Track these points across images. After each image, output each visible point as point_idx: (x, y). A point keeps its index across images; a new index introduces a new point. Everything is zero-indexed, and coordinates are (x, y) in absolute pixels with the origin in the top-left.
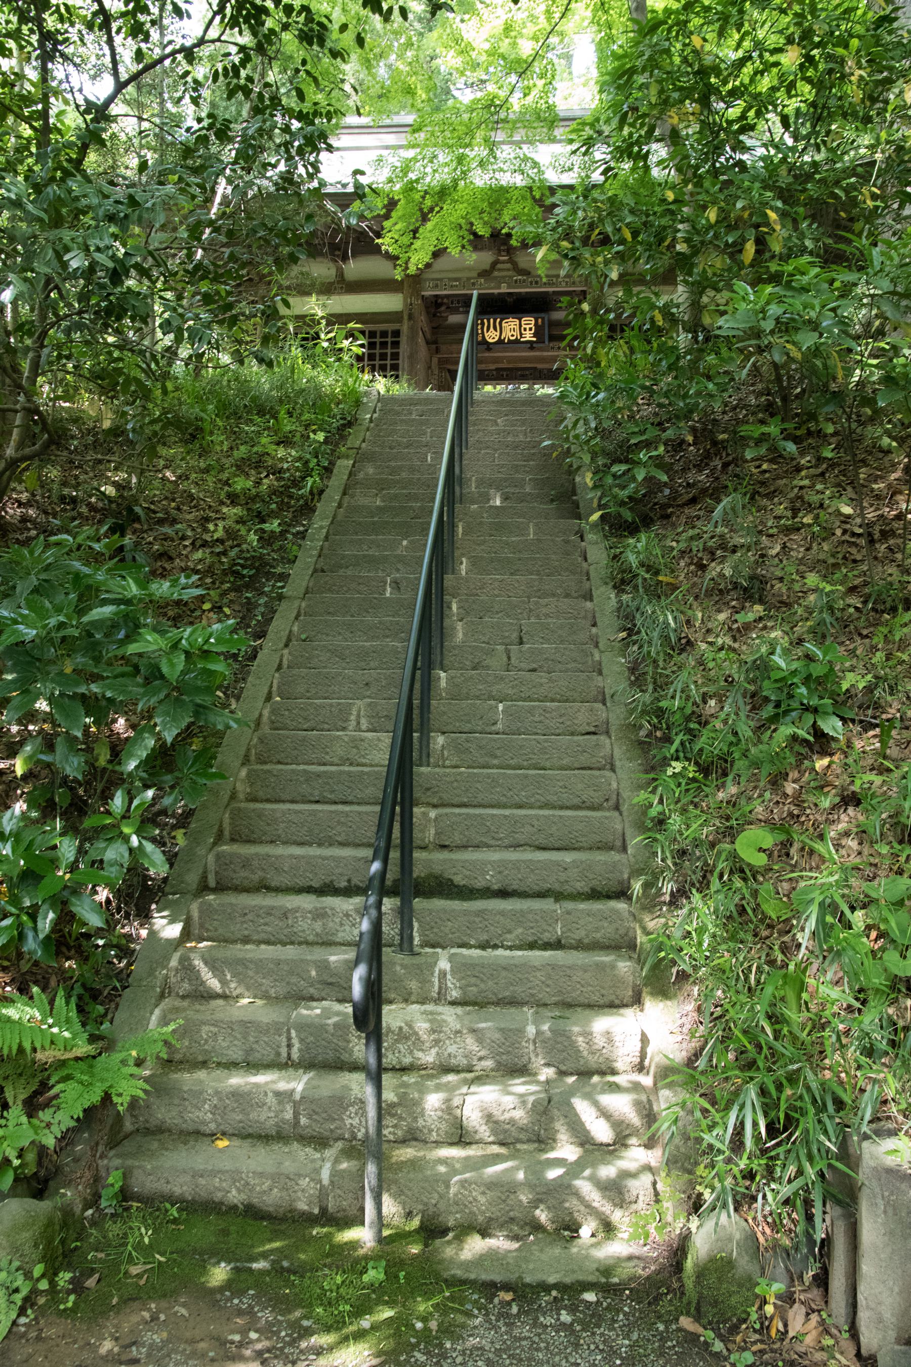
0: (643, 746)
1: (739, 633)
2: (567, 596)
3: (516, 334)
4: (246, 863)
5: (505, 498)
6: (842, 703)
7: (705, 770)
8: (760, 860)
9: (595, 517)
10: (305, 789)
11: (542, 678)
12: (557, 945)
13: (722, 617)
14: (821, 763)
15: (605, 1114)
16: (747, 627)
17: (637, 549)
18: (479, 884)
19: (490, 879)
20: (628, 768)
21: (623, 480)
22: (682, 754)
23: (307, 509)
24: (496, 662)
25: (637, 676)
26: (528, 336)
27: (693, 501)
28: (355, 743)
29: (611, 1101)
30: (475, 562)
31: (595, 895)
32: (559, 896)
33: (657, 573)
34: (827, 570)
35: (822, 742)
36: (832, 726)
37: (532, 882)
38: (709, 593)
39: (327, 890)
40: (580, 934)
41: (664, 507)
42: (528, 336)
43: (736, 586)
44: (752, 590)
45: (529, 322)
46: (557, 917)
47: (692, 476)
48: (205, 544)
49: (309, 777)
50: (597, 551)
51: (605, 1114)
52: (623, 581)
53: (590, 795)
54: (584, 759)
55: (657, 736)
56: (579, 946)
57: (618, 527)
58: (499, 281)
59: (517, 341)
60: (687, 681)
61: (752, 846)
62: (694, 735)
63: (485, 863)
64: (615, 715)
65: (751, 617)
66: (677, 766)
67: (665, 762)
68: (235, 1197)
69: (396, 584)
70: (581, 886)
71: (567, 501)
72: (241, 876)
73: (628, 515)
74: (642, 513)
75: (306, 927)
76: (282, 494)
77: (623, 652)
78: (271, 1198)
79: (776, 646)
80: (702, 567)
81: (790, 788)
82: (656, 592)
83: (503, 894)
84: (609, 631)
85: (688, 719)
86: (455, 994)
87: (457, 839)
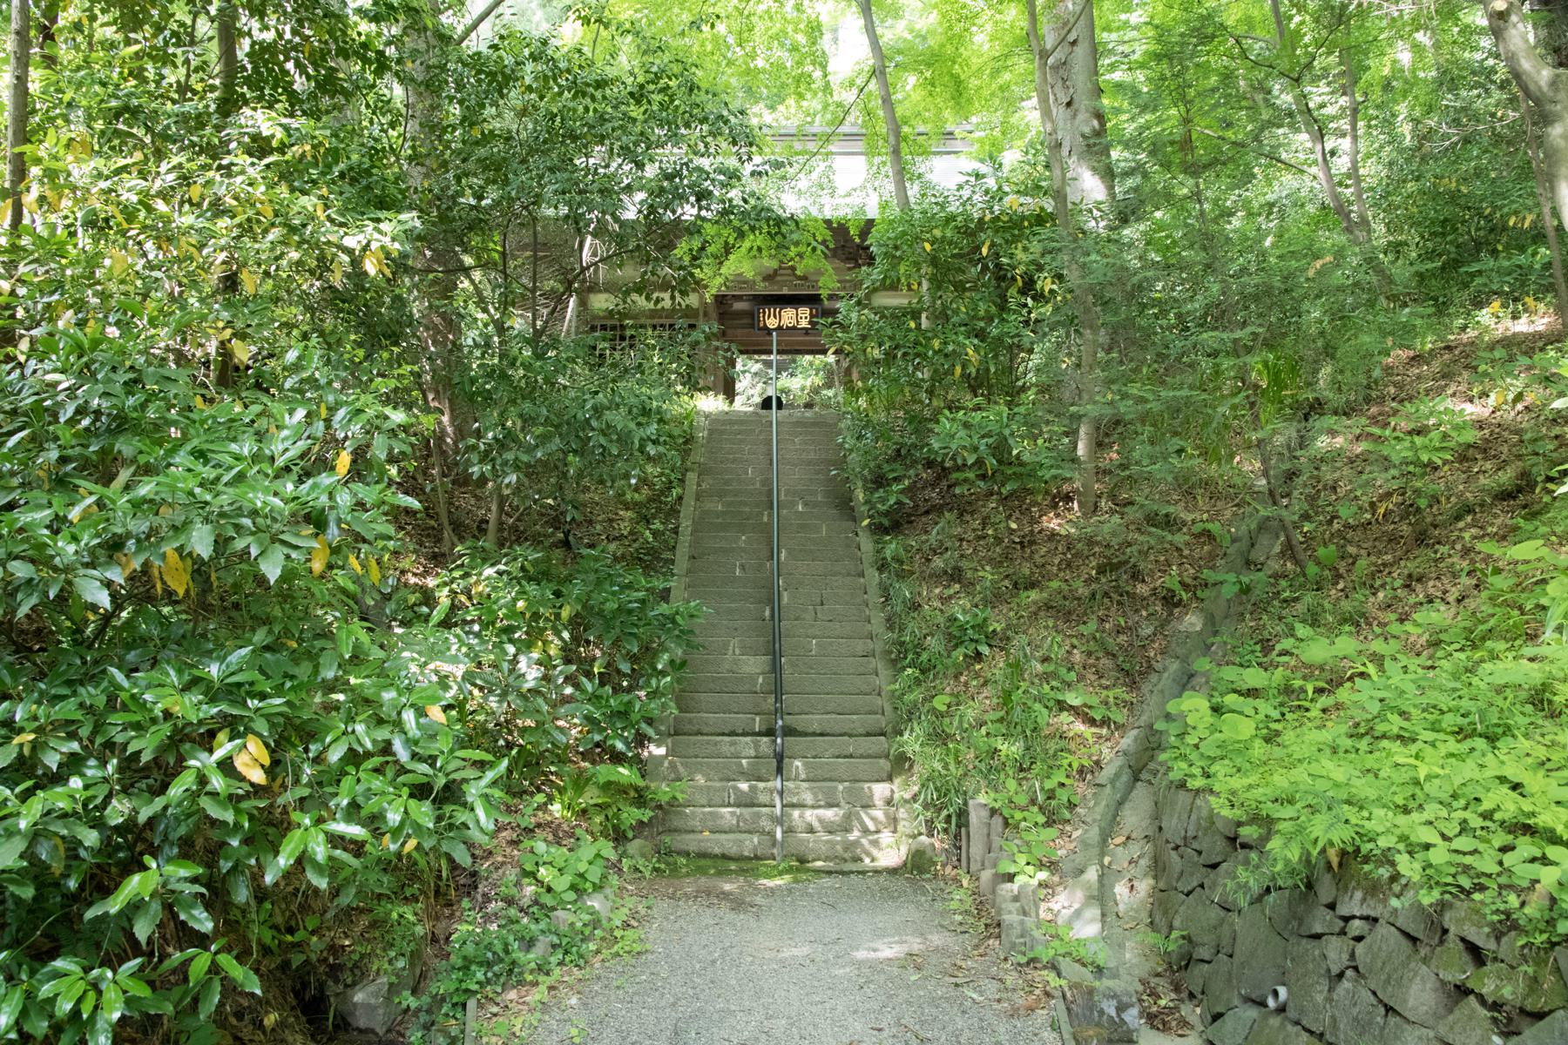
0: (894, 662)
1: (945, 600)
2: (849, 574)
3: (794, 322)
4: (690, 721)
5: (806, 504)
6: (990, 638)
7: (923, 672)
8: (944, 708)
9: (866, 522)
10: (712, 686)
11: (837, 615)
12: (851, 756)
13: (937, 591)
14: (978, 667)
15: (873, 819)
16: (950, 597)
17: (892, 547)
18: (811, 730)
19: (816, 727)
20: (885, 672)
21: (883, 500)
22: (912, 665)
23: (674, 512)
24: (809, 616)
25: (890, 623)
26: (804, 324)
27: (927, 512)
28: (736, 662)
29: (874, 812)
30: (789, 552)
31: (868, 734)
32: (850, 736)
33: (902, 563)
34: (996, 564)
35: (978, 656)
36: (985, 650)
37: (837, 729)
38: (931, 576)
39: (733, 734)
40: (861, 751)
41: (909, 515)
42: (804, 324)
43: (946, 572)
44: (955, 575)
45: (804, 312)
46: (851, 745)
47: (928, 493)
48: (615, 539)
49: (714, 680)
50: (867, 544)
51: (873, 819)
52: (882, 567)
53: (864, 688)
54: (861, 670)
55: (899, 656)
56: (861, 757)
57: (879, 530)
58: (783, 284)
59: (794, 328)
60: (914, 627)
61: (940, 703)
62: (919, 655)
63: (814, 722)
64: (878, 646)
65: (952, 591)
66: (910, 671)
67: (904, 669)
68: (717, 851)
69: (743, 567)
70: (861, 731)
71: (844, 505)
72: (688, 727)
73: (886, 522)
74: (893, 524)
75: (726, 749)
76: (654, 499)
77: (882, 610)
78: (733, 850)
79: (962, 609)
80: (929, 560)
81: (963, 679)
82: (902, 576)
83: (822, 735)
84: (875, 598)
85: (916, 647)
86: (803, 776)
87: (796, 709)
